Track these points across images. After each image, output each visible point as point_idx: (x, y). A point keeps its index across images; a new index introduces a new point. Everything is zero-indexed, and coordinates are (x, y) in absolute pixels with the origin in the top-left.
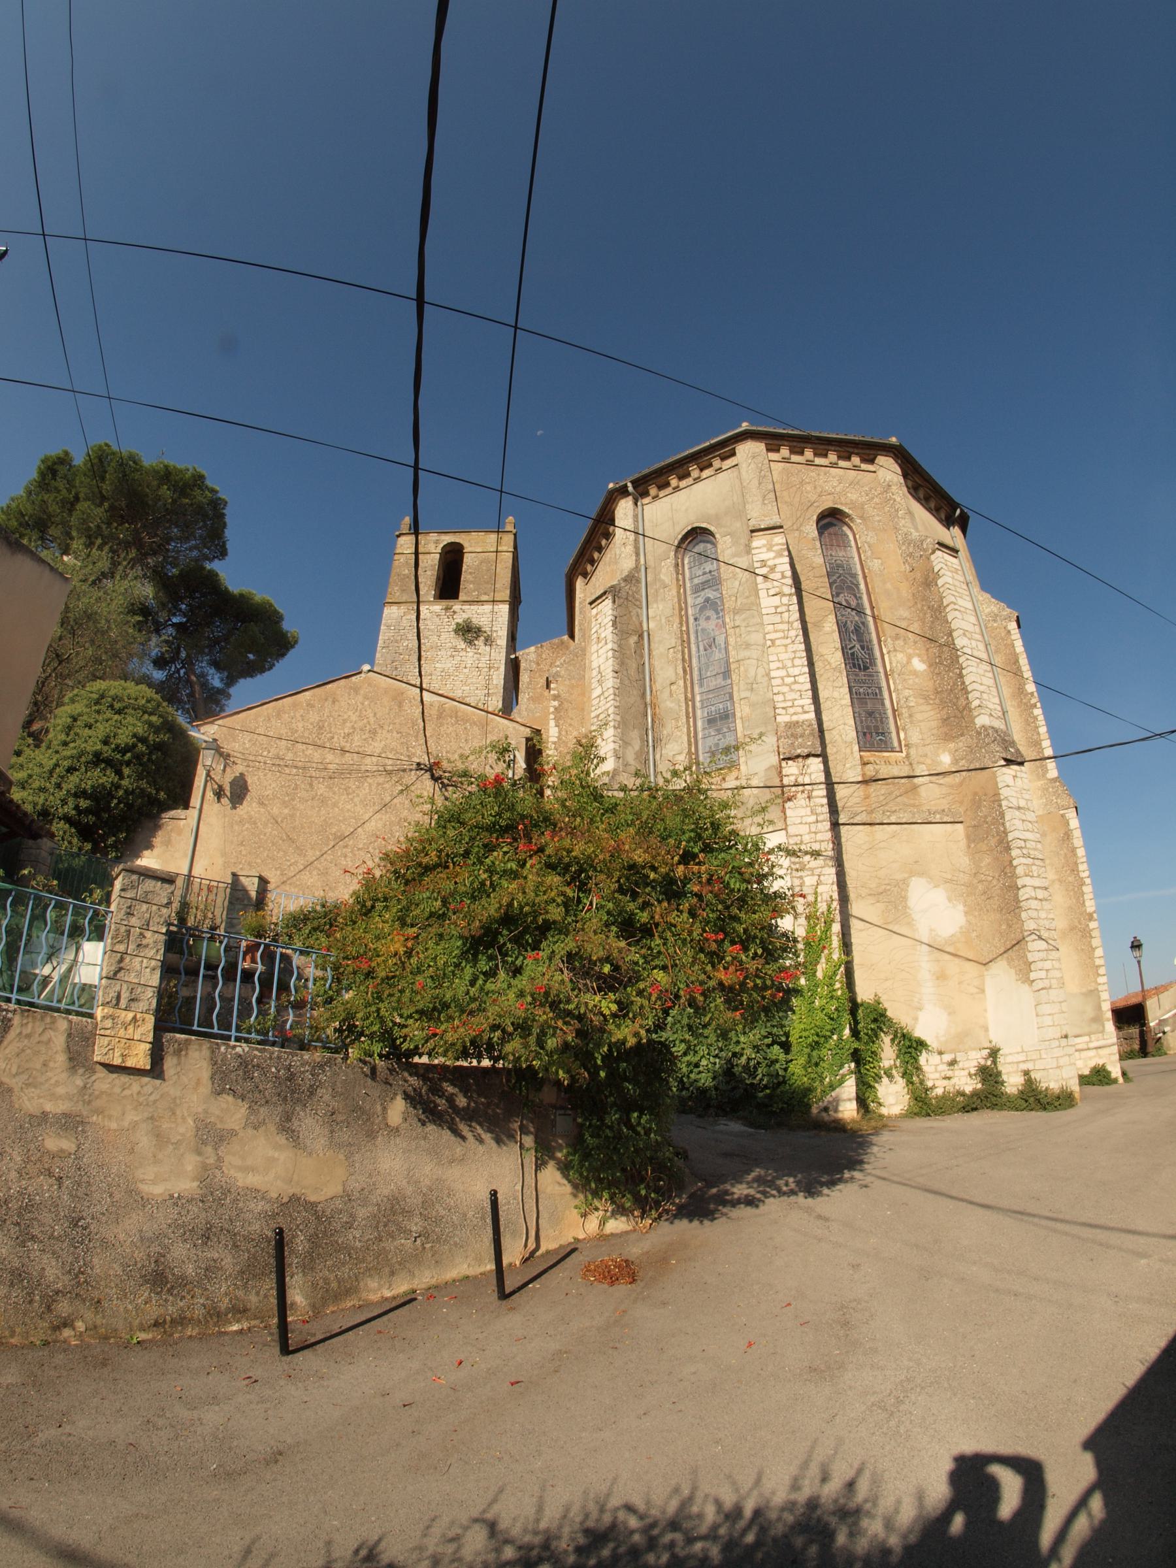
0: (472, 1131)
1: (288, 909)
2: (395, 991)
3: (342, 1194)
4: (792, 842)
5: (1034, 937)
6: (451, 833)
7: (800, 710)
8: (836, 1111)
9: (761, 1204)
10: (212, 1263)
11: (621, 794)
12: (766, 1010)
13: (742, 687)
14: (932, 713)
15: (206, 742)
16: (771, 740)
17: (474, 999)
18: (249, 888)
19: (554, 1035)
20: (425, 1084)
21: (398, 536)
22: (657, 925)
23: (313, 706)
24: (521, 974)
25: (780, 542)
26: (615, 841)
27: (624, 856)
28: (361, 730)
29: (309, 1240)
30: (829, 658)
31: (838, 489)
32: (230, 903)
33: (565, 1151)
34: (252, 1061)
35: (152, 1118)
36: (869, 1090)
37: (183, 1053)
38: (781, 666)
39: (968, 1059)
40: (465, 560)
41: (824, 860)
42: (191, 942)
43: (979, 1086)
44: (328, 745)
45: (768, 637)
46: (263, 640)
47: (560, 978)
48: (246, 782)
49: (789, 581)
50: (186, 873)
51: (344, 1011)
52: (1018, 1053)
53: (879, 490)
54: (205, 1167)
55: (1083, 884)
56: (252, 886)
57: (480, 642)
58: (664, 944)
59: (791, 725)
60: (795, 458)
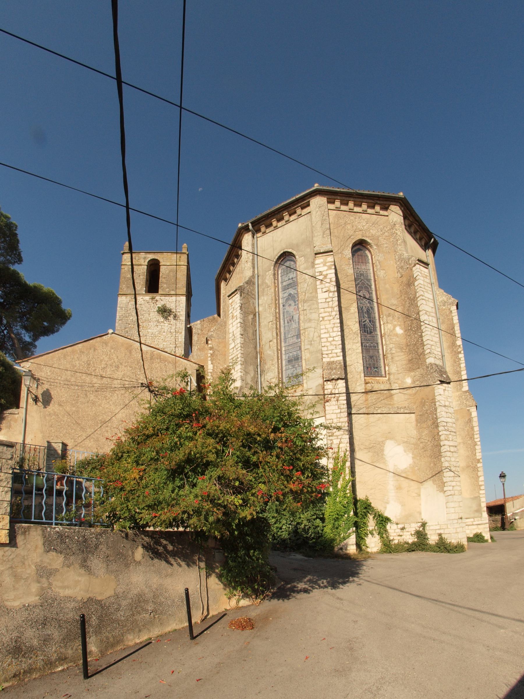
0: (176, 561)
1: (78, 459)
2: (135, 497)
3: (114, 595)
4: (328, 422)
5: (447, 470)
6: (159, 418)
7: (335, 355)
8: (346, 549)
9: (311, 592)
10: (48, 637)
11: (243, 399)
12: (313, 502)
13: (306, 343)
14: (404, 356)
15: (24, 372)
16: (319, 371)
17: (174, 499)
18: (57, 449)
19: (212, 515)
20: (152, 540)
21: (123, 254)
22: (261, 462)
23: (83, 352)
24: (196, 487)
25: (331, 260)
26: (240, 422)
27: (245, 429)
28: (111, 365)
29: (98, 619)
30: (352, 327)
31: (365, 228)
32: (47, 456)
33: (220, 569)
34: (65, 534)
35: (11, 567)
36: (362, 540)
37: (27, 533)
38: (327, 332)
39: (410, 527)
40: (161, 270)
41: (343, 431)
42: (27, 477)
43: (416, 540)
44: (93, 374)
45: (321, 315)
46: (51, 315)
47: (215, 488)
48: (50, 394)
49: (334, 284)
50: (22, 442)
51: (110, 507)
52: (436, 525)
53: (389, 227)
54: (42, 589)
55: (476, 444)
56: (59, 448)
57: (171, 318)
58: (264, 472)
59: (329, 363)
60: (343, 208)
